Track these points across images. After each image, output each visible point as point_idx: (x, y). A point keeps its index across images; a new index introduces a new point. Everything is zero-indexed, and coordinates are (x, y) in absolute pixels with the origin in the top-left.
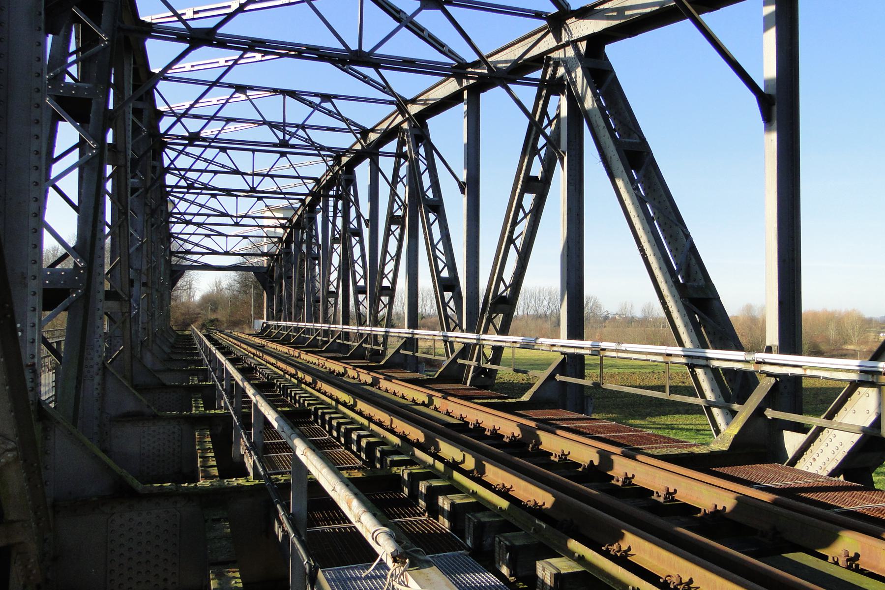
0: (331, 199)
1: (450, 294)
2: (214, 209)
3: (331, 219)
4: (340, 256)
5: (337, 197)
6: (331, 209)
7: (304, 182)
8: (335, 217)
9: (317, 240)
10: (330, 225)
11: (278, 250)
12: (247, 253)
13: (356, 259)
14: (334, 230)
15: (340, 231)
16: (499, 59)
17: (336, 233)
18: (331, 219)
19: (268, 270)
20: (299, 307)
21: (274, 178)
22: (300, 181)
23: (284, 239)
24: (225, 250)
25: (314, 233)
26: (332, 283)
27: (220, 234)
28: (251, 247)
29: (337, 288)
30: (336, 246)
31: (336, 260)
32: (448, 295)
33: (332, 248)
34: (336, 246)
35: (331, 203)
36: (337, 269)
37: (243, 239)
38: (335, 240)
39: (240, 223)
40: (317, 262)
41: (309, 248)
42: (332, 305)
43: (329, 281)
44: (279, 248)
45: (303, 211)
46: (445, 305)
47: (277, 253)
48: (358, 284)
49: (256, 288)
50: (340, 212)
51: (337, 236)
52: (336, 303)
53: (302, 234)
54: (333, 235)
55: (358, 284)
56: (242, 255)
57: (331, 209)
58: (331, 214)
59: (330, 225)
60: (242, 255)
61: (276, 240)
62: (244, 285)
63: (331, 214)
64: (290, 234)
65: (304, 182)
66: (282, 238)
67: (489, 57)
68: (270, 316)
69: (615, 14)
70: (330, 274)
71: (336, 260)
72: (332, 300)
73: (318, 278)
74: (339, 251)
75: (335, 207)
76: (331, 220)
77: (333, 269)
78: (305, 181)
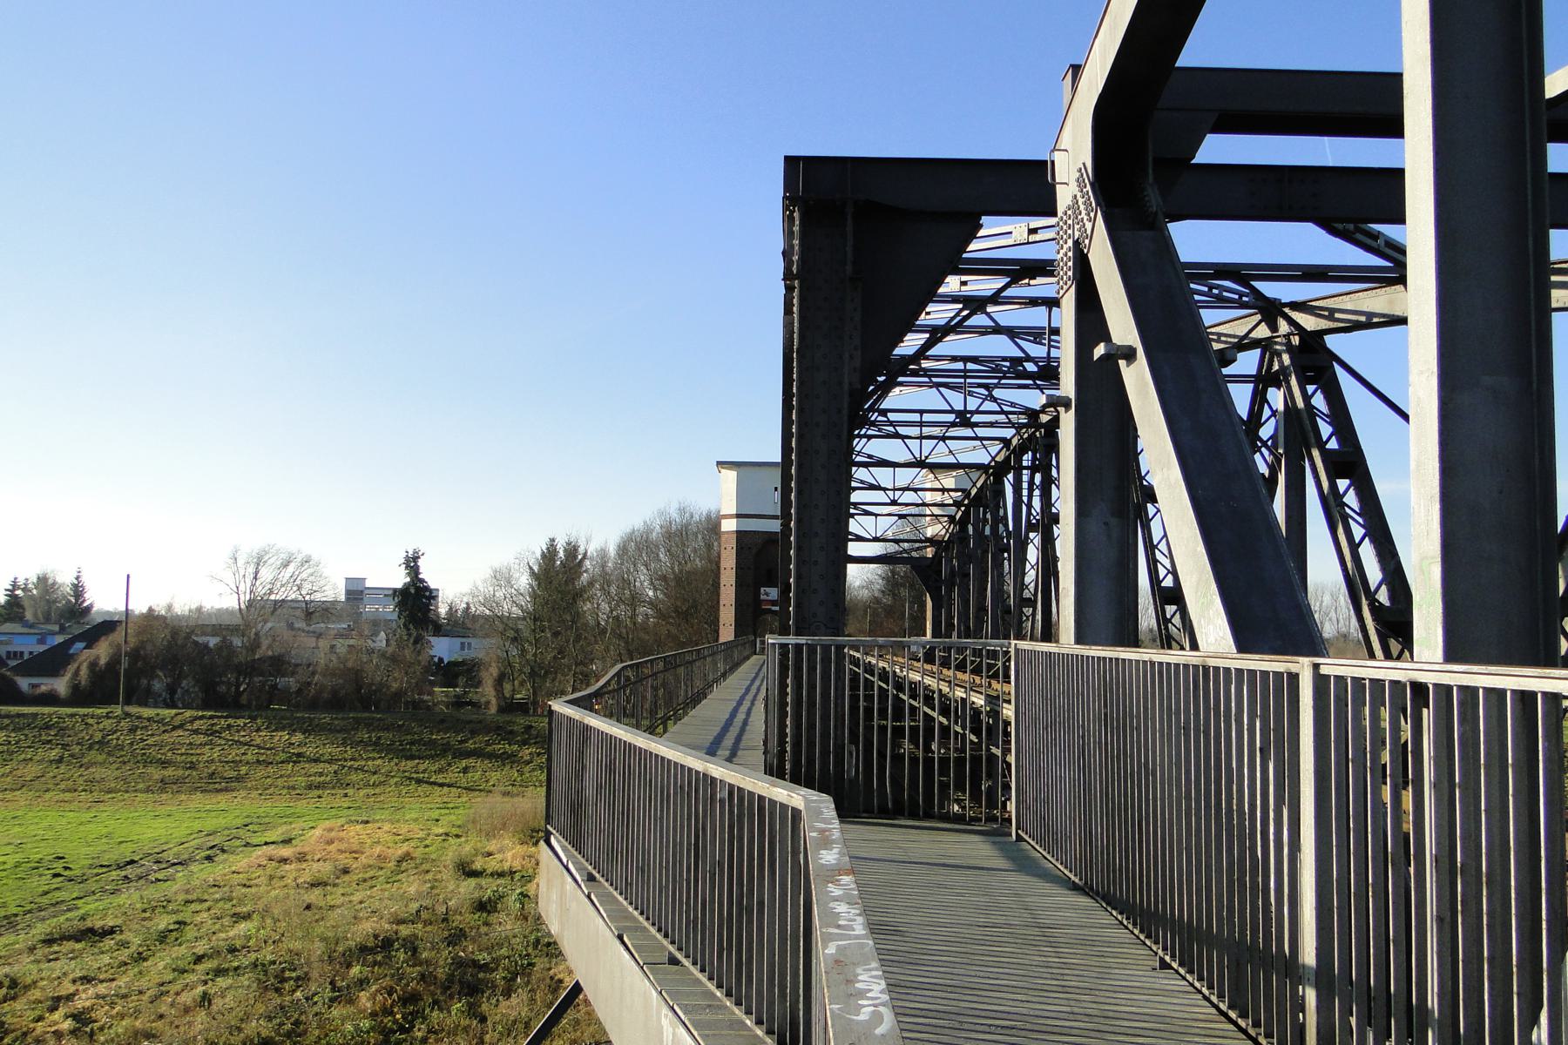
0: (1025, 472)
1: (1174, 608)
2: (861, 481)
3: (1025, 499)
4: (1038, 549)
5: (1033, 469)
6: (1025, 485)
7: (983, 444)
8: (1030, 496)
9: (1006, 525)
10: (1024, 508)
11: (948, 535)
12: (906, 538)
13: (1026, 583)
14: (1029, 513)
15: (1038, 514)
16: (1225, 332)
17: (1032, 517)
18: (1025, 499)
19: (932, 563)
20: (980, 621)
21: (947, 441)
22: (978, 443)
23: (958, 517)
24: (874, 536)
25: (1001, 512)
26: (1027, 586)
27: (867, 513)
28: (908, 530)
29: (1035, 594)
30: (1032, 535)
31: (1033, 554)
32: (1170, 609)
33: (1027, 537)
34: (1032, 535)
35: (1025, 478)
36: (1035, 567)
37: (899, 518)
38: (1031, 527)
39: (899, 502)
40: (1006, 555)
41: (994, 529)
42: (1028, 617)
43: (1023, 584)
44: (950, 531)
45: (985, 481)
46: (1167, 621)
47: (946, 539)
48: (1163, 585)
49: (912, 586)
50: (1037, 487)
51: (1034, 521)
52: (1034, 614)
53: (985, 513)
54: (1028, 520)
55: (1163, 585)
56: (897, 541)
57: (1025, 485)
58: (1025, 492)
59: (1024, 508)
60: (897, 541)
61: (946, 519)
62: (892, 584)
63: (1025, 492)
64: (966, 514)
65: (983, 444)
66: (954, 517)
67: (1210, 327)
68: (729, 741)
69: (1326, 313)
70: (1024, 574)
71: (1033, 554)
72: (1028, 611)
73: (1007, 578)
74: (1036, 541)
75: (1031, 482)
76: (1026, 501)
77: (1028, 566)
78: (984, 442)
